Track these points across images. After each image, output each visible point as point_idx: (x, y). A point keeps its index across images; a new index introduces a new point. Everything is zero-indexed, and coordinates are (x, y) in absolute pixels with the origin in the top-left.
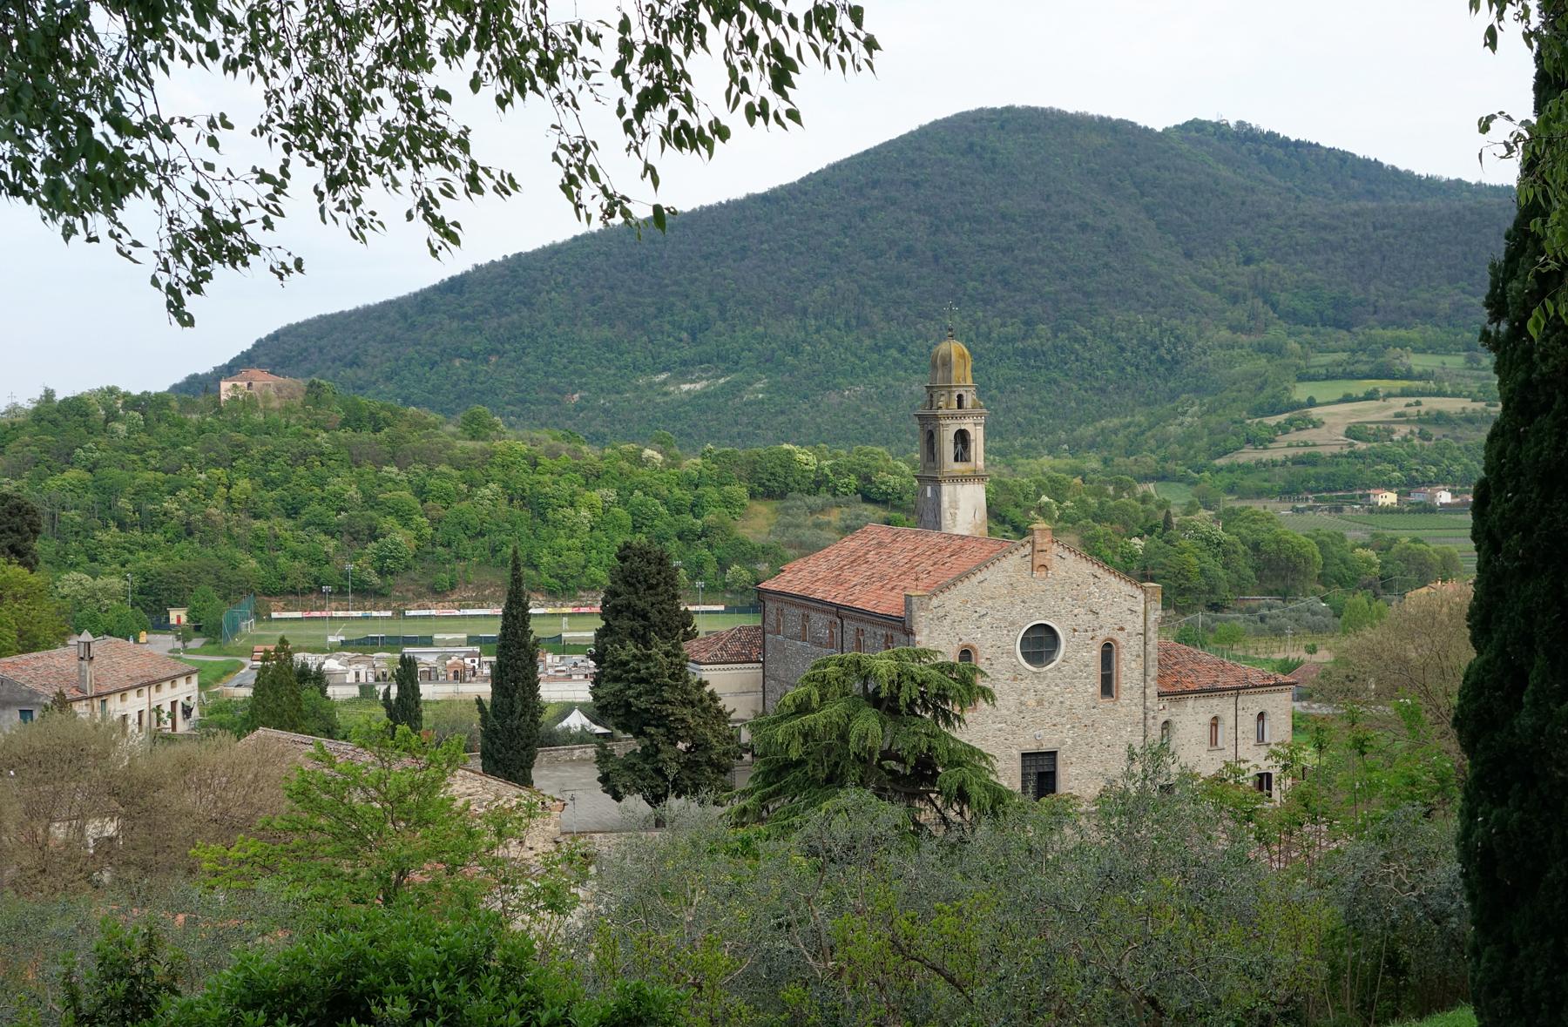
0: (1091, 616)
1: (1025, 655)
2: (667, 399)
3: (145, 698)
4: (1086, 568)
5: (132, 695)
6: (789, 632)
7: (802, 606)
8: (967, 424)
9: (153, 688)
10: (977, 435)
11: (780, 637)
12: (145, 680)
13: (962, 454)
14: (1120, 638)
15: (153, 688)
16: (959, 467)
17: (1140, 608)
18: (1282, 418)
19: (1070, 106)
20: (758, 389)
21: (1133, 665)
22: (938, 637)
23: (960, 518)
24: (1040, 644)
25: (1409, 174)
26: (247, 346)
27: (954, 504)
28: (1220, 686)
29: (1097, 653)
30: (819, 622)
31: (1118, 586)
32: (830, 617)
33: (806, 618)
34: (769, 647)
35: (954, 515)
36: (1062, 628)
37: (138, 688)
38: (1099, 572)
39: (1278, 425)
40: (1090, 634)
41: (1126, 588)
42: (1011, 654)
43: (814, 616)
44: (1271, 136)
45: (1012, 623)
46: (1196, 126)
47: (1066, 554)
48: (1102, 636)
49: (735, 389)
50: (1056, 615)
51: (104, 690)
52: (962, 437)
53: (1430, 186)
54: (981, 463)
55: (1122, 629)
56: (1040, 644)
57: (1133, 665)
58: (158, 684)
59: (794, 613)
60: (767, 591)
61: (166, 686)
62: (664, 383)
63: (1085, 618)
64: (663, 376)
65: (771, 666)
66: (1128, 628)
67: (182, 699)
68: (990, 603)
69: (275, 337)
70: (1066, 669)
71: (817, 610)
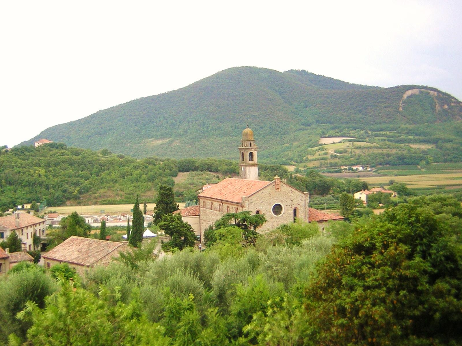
0: (291, 201)
1: (273, 212)
2: (153, 145)
3: (41, 226)
4: (290, 189)
5: (29, 228)
6: (207, 207)
7: (211, 200)
8: (253, 151)
9: (35, 226)
10: (255, 154)
11: (204, 209)
12: (33, 224)
13: (251, 159)
14: (298, 207)
15: (35, 226)
16: (251, 162)
17: (303, 199)
18: (317, 148)
19: (259, 66)
20: (177, 143)
21: (302, 214)
22: (251, 209)
23: (251, 176)
24: (277, 209)
25: (348, 83)
26: (39, 133)
27: (250, 172)
28: (325, 219)
29: (292, 211)
30: (216, 204)
31: (297, 193)
32: (219, 203)
33: (212, 203)
34: (201, 211)
35: (250, 175)
36: (283, 205)
37: (31, 226)
38: (293, 190)
39: (316, 150)
40: (290, 206)
41: (300, 194)
42: (270, 212)
43: (214, 203)
44: (312, 74)
45: (270, 204)
46: (292, 71)
47: (284, 185)
48: (293, 207)
49: (170, 143)
50: (282, 202)
51: (22, 226)
52: (251, 154)
53: (353, 86)
54: (256, 161)
55: (299, 205)
56: (277, 209)
57: (302, 214)
58: (35, 225)
59: (208, 202)
60: (200, 196)
61: (38, 225)
62: (152, 141)
63: (289, 202)
64: (151, 139)
65: (202, 217)
66: (301, 204)
67: (42, 228)
68: (264, 198)
69: (46, 131)
70: (284, 216)
71: (215, 201)
